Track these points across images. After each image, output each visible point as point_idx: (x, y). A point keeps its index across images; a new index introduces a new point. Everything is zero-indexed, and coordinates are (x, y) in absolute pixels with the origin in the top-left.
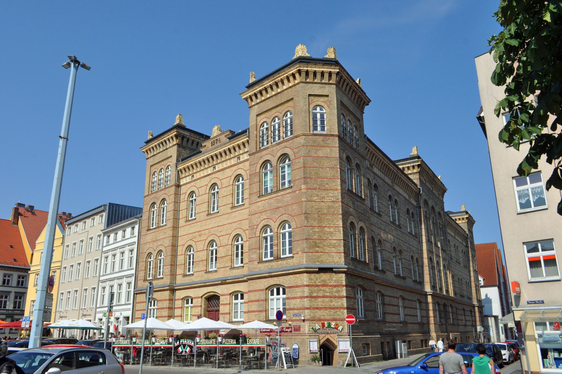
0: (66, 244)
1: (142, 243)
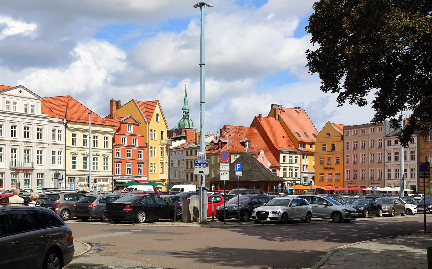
0: (345, 142)
1: (421, 147)
